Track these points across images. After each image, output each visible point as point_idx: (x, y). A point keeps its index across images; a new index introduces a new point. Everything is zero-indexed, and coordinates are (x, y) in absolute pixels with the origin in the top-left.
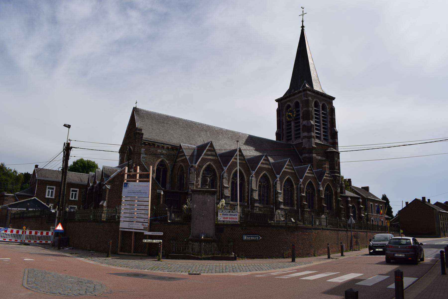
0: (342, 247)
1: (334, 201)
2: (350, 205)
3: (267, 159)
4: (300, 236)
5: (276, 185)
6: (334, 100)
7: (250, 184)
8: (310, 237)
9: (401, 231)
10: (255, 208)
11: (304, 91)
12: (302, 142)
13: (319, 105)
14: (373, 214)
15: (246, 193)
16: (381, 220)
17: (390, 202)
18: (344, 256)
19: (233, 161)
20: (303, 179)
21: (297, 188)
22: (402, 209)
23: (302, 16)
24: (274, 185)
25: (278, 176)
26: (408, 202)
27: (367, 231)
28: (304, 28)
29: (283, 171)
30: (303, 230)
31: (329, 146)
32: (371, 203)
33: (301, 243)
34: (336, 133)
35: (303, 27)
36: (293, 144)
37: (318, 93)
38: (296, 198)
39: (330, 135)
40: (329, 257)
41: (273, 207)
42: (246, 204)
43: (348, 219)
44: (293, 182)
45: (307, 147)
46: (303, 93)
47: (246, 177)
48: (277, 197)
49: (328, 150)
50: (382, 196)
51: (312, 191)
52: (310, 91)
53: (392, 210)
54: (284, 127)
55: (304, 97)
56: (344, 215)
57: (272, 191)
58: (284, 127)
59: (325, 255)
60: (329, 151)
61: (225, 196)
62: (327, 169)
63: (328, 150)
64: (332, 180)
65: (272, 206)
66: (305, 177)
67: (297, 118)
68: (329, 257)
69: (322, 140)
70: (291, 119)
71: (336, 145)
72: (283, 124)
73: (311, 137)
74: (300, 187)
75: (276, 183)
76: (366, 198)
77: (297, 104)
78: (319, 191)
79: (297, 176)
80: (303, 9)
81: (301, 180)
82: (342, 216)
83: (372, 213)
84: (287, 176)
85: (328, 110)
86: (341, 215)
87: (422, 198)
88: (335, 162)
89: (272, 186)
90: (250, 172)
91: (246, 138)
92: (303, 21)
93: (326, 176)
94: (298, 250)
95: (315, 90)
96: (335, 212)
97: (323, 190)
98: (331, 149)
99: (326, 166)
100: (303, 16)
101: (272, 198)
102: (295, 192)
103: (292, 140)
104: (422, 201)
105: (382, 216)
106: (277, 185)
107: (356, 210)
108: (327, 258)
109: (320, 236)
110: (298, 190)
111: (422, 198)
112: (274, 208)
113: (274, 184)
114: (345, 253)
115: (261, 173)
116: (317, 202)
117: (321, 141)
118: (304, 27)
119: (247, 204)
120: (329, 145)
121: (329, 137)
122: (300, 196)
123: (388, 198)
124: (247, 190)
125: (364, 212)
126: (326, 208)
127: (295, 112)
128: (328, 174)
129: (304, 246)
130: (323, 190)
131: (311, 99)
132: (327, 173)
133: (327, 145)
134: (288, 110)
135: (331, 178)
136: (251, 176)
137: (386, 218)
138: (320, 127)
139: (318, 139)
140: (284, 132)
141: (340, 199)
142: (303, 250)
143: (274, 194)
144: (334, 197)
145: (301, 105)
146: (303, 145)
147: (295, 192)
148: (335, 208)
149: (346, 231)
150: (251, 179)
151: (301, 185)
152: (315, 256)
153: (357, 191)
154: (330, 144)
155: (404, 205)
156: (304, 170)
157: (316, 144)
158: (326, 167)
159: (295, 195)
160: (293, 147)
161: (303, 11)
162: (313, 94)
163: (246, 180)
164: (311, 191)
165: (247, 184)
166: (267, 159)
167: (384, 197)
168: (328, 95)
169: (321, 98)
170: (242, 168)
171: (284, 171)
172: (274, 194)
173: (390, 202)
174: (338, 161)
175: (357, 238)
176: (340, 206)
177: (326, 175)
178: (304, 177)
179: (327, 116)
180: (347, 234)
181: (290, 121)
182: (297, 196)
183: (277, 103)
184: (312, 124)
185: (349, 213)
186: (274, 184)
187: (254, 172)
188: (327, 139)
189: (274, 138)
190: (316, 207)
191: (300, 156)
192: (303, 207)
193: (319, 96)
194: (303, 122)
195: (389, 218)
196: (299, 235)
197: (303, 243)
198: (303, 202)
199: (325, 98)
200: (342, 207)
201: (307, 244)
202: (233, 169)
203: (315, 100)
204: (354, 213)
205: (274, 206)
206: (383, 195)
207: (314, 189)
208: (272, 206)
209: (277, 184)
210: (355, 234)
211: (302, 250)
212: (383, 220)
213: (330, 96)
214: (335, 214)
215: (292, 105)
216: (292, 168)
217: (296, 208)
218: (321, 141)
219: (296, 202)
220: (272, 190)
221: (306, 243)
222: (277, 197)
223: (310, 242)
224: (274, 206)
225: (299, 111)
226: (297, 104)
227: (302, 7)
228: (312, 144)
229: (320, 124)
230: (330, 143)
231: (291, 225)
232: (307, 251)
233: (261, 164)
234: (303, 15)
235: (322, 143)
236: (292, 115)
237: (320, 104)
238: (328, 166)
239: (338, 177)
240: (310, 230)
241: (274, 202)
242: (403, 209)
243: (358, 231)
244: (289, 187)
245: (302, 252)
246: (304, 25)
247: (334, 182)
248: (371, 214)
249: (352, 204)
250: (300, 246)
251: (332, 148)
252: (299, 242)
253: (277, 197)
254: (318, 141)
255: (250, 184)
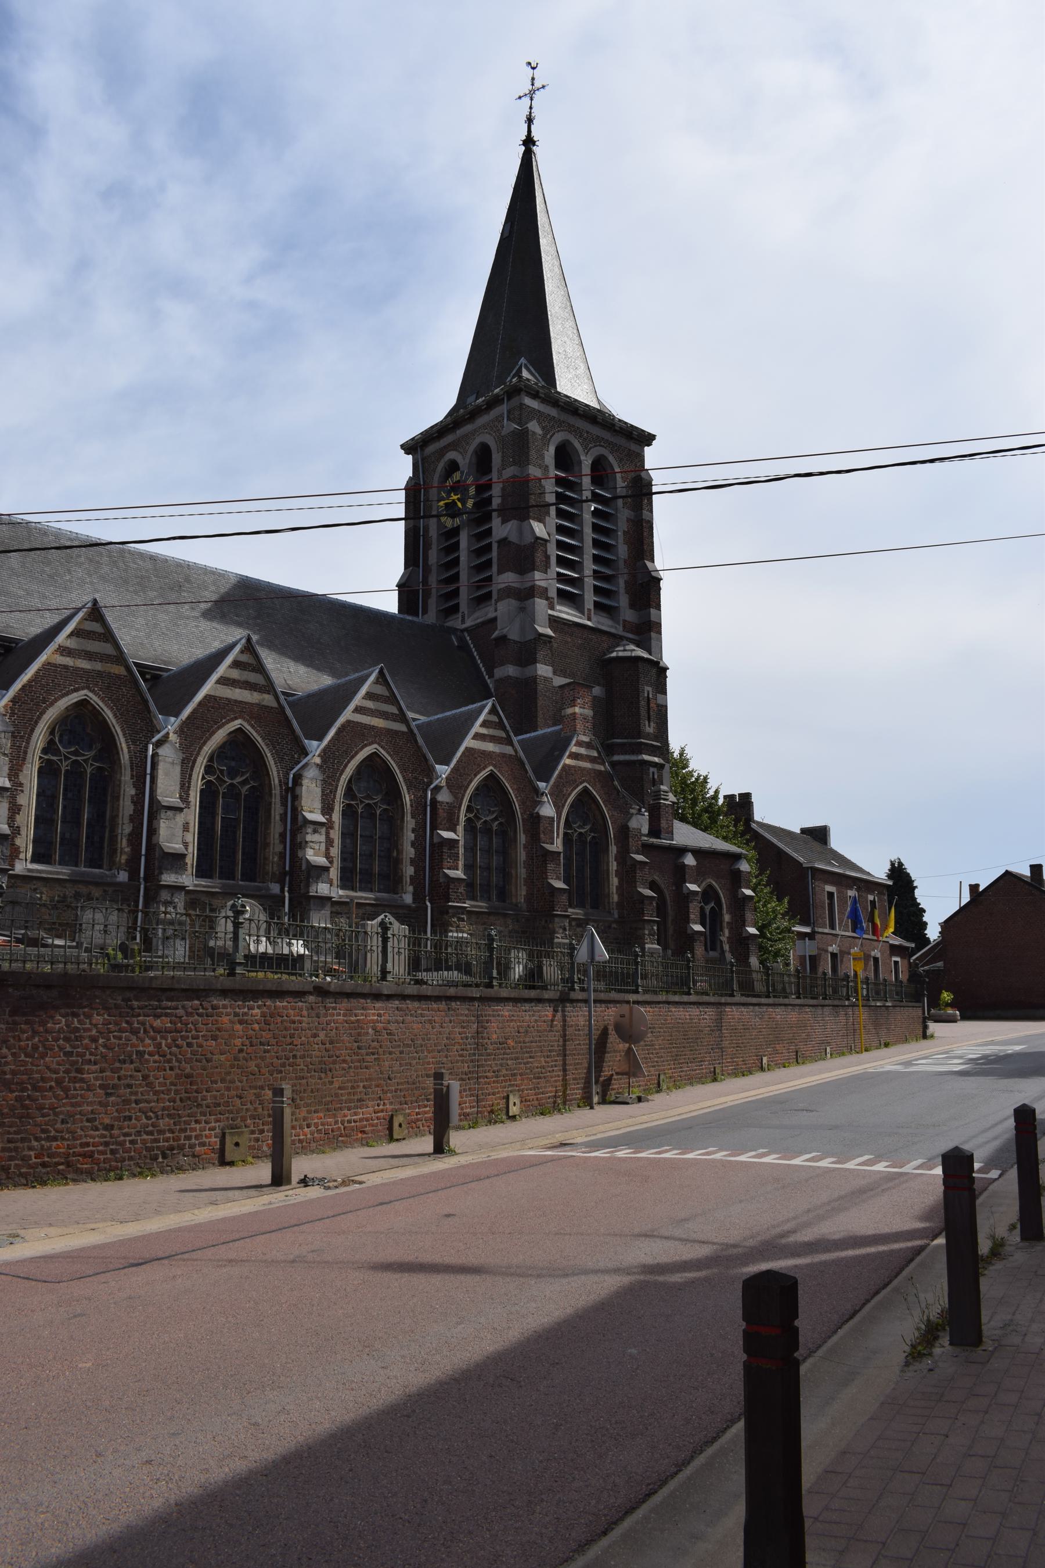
0: (442, 1102)
1: (615, 868)
2: (693, 887)
3: (252, 661)
4: (94, 1040)
5: (298, 788)
6: (649, 445)
7: (148, 777)
8: (189, 1045)
9: (946, 996)
10: (165, 895)
11: (509, 399)
12: (495, 619)
13: (580, 462)
14: (837, 931)
15: (126, 820)
16: (873, 954)
17: (916, 887)
18: (452, 1152)
19: (48, 664)
20: (452, 765)
21: (419, 807)
22: (958, 908)
23: (526, 101)
24: (288, 790)
25: (315, 743)
26: (977, 886)
27: (723, 1000)
28: (534, 148)
29: (341, 720)
30: (127, 1000)
31: (622, 638)
32: (829, 888)
33: (101, 1086)
34: (655, 582)
35: (529, 142)
36: (464, 626)
37: (572, 408)
38: (409, 852)
39: (627, 593)
40: (280, 1178)
41: (282, 891)
42: (123, 876)
43: (580, 938)
44: (400, 778)
45: (514, 635)
46: (504, 408)
47: (124, 746)
48: (301, 843)
49: (614, 654)
50: (889, 866)
51: (501, 820)
52: (535, 396)
53: (925, 919)
54: (433, 556)
55: (509, 419)
56: (655, 928)
57: (278, 818)
58: (433, 556)
59: (419, 1134)
60: (619, 659)
61: (163, 850)
62: (579, 726)
63: (612, 652)
64: (606, 771)
65: (275, 888)
66: (463, 753)
67: (482, 514)
68: (280, 1178)
69: (589, 610)
70: (457, 521)
71: (653, 635)
72: (427, 546)
73: (529, 593)
74: (434, 801)
75: (298, 779)
76: (808, 868)
77: (483, 455)
78: (535, 821)
79: (419, 748)
80: (534, 68)
81: (443, 771)
82: (647, 932)
83: (833, 927)
84: (366, 746)
85: (620, 483)
86: (644, 929)
87: (1032, 866)
88: (643, 703)
89: (276, 791)
90: (152, 721)
91: (223, 590)
92: (530, 120)
93: (575, 756)
94: (69, 1131)
95: (559, 393)
96: (616, 916)
97: (559, 818)
98: (627, 648)
99: (577, 710)
100: (532, 99)
101: (279, 848)
102: (410, 823)
103: (461, 610)
104: (1029, 880)
105: (834, 932)
106: (304, 788)
107: (724, 906)
108: (269, 1181)
109: (292, 1036)
110: (425, 814)
111: (1032, 866)
112: (287, 894)
113: (290, 785)
114: (456, 1139)
115: (219, 728)
116: (523, 871)
117: (582, 612)
118: (534, 143)
119: (130, 879)
120: (619, 630)
121: (623, 601)
122: (432, 844)
123: (909, 874)
124: (127, 808)
125: (789, 920)
126: (564, 898)
127: (472, 491)
128: (588, 745)
129: (127, 1102)
130: (559, 818)
131: (539, 431)
132: (579, 744)
133: (613, 631)
134: (449, 482)
135: (603, 764)
136: (154, 740)
137: (892, 946)
138: (581, 555)
139: (569, 607)
140: (433, 580)
141: (640, 858)
142: (115, 1132)
143: (289, 827)
144: (613, 849)
145: (496, 458)
146: (499, 628)
147: (410, 823)
148: (616, 898)
149: (550, 1001)
150: (155, 755)
151: (438, 788)
152: (231, 1164)
153: (775, 841)
154: (624, 626)
155: (966, 898)
156: (462, 726)
157: (555, 622)
158: (575, 713)
159: (409, 836)
160: (462, 640)
161: (533, 79)
162: (553, 412)
163: (127, 756)
164: (496, 819)
165: (132, 776)
166: (252, 661)
167: (898, 871)
168: (620, 420)
169: (588, 432)
170: (102, 699)
171: (349, 722)
172: (289, 827)
173: (916, 887)
174: (660, 701)
175: (630, 1036)
176: (639, 890)
177: (573, 749)
178: (459, 754)
179: (616, 510)
180: (564, 1021)
181: (455, 532)
182: (416, 844)
183: (410, 457)
184: (538, 535)
185: (687, 921)
186: (288, 783)
187: (173, 719)
188: (617, 607)
189: (389, 603)
190: (521, 893)
191: (487, 677)
192: (442, 890)
193: (580, 423)
194: (500, 529)
195: (907, 948)
196: (90, 1030)
197: (114, 1087)
198: (446, 871)
199: (606, 435)
200: (648, 892)
201: (156, 1093)
202: (52, 704)
203: (559, 437)
204: (712, 921)
205: (286, 889)
206: (892, 864)
207: (512, 813)
208: (275, 888)
209: (305, 782)
210: (622, 1016)
211: (109, 1128)
212: (878, 955)
213: (632, 426)
214: (614, 926)
215: (464, 459)
216: (393, 710)
217: (408, 899)
218: (583, 614)
219: (409, 871)
220: (277, 810)
221: (150, 1085)
222: (298, 846)
223: (188, 1076)
224: (286, 889)
225: (488, 486)
226: (483, 455)
227: (529, 64)
228: (533, 621)
229: (581, 541)
230: (627, 626)
231: (28, 966)
232: (151, 1133)
233: (218, 682)
234: (531, 95)
235: (589, 623)
236: (459, 505)
237: (583, 458)
238: (589, 712)
239: (652, 769)
240: (189, 1004)
241: (287, 868)
242: (962, 910)
243: (637, 1002)
244: (378, 798)
245: (106, 1144)
246: (533, 134)
247: (616, 783)
248: (827, 931)
249: (704, 884)
250: (89, 1104)
251: (632, 647)
252: (82, 1080)
253: (301, 843)
254: (566, 613)
255: (148, 777)
